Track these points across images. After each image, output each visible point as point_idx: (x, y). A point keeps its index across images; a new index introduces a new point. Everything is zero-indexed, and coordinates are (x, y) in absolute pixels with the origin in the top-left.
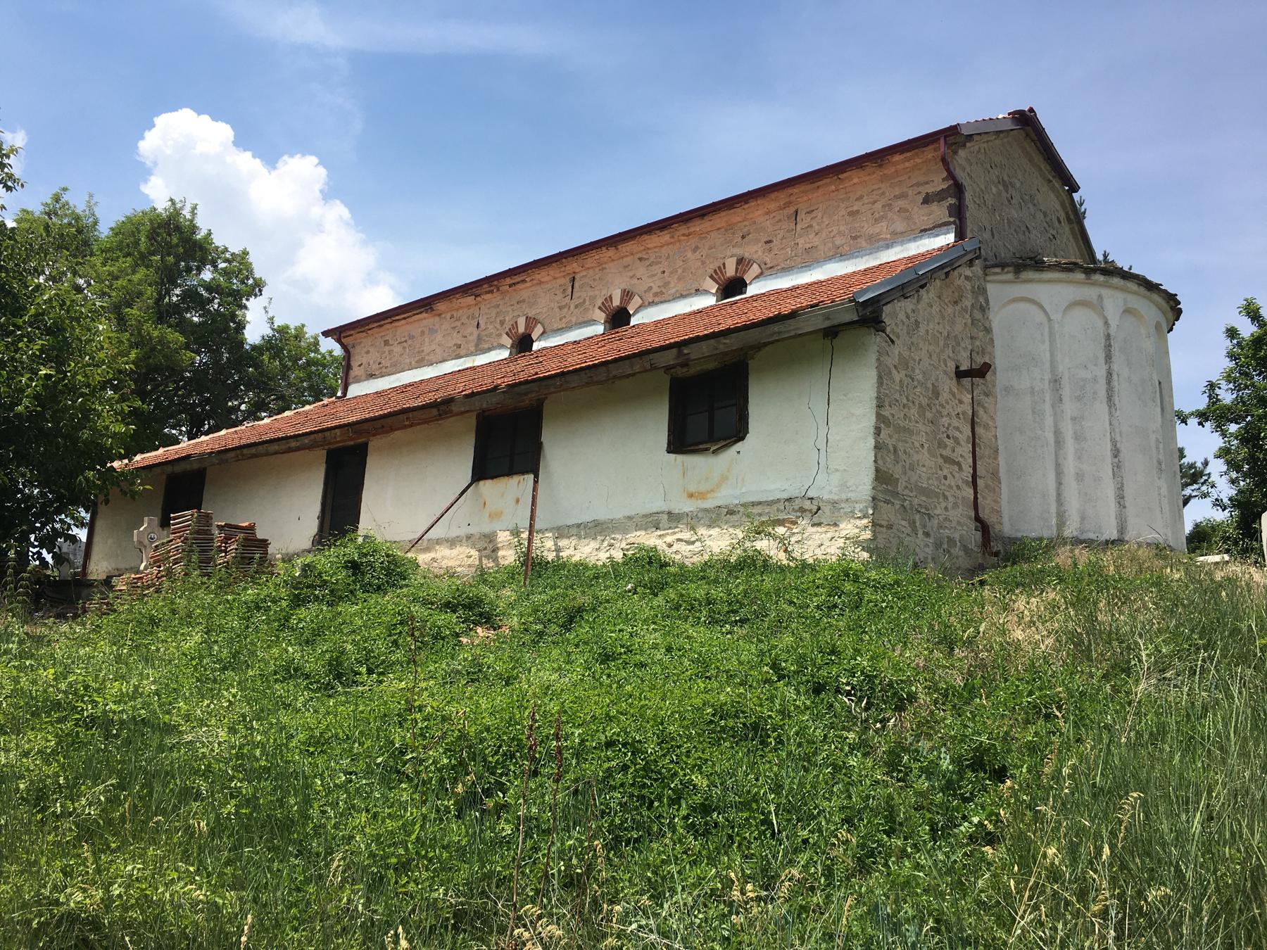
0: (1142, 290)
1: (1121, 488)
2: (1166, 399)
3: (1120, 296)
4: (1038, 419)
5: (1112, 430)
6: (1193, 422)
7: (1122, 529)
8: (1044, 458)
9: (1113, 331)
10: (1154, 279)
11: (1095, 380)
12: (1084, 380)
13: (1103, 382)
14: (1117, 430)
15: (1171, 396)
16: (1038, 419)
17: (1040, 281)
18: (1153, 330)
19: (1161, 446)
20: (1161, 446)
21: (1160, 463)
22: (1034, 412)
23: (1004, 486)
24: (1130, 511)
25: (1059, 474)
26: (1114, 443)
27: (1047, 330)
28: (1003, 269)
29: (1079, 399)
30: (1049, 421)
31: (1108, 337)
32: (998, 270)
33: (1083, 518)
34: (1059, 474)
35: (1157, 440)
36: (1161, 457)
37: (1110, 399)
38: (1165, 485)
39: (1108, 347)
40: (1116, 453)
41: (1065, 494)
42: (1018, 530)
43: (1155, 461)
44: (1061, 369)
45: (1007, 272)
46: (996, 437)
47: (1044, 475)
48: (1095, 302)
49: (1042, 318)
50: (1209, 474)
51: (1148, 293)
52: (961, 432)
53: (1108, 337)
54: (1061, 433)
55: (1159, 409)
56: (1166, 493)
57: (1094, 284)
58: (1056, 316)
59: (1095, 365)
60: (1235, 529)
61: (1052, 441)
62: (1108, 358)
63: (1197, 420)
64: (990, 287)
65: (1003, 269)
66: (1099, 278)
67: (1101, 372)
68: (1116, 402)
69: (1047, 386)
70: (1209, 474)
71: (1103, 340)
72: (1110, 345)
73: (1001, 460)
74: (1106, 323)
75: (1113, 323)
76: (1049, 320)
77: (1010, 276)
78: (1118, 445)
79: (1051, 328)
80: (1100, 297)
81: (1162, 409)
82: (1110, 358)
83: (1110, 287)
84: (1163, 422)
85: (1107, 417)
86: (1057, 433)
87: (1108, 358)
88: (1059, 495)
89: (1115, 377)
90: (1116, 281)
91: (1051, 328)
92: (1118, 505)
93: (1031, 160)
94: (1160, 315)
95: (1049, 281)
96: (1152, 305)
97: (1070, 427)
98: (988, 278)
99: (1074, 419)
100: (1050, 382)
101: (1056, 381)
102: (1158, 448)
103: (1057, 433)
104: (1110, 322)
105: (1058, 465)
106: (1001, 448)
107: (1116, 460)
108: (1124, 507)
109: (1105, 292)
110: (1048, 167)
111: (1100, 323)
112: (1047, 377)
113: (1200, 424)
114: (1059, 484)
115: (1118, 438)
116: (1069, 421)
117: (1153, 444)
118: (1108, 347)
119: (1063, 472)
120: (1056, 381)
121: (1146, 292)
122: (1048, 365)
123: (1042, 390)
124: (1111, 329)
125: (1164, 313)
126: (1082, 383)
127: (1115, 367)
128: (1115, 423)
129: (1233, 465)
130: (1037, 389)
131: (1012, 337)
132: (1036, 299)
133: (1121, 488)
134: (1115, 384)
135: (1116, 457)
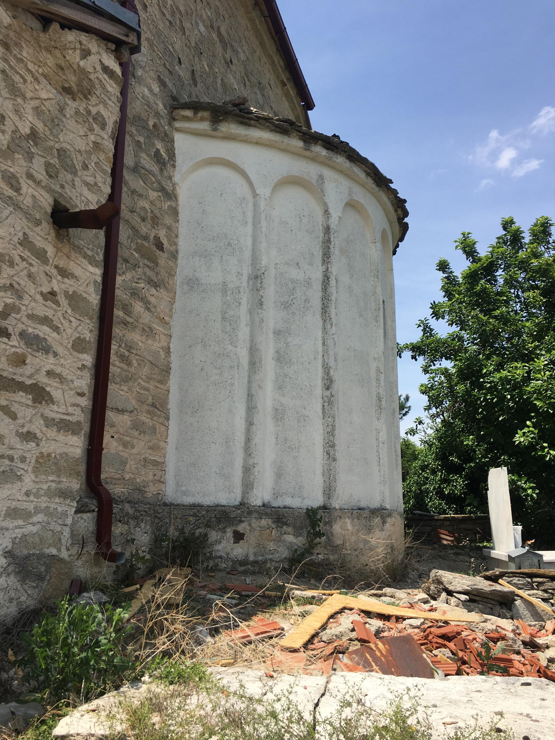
0: (370, 182)
1: (331, 433)
2: (389, 322)
3: (345, 184)
4: (228, 329)
5: (325, 352)
6: (407, 354)
7: (329, 491)
8: (232, 385)
9: (334, 222)
10: (385, 170)
11: (308, 283)
12: (293, 281)
13: (317, 286)
14: (331, 352)
15: (394, 321)
16: (228, 329)
17: (246, 141)
18: (378, 236)
19: (382, 377)
20: (382, 377)
21: (379, 399)
22: (224, 319)
23: (173, 425)
24: (342, 464)
25: (251, 409)
26: (326, 369)
27: (251, 205)
28: (195, 113)
29: (286, 306)
30: (244, 332)
31: (327, 230)
32: (188, 113)
33: (279, 475)
34: (251, 409)
35: (378, 371)
36: (381, 391)
37: (325, 310)
38: (384, 429)
39: (327, 243)
40: (328, 384)
41: (257, 439)
42: (184, 493)
43: (375, 398)
44: (264, 261)
45: (202, 119)
46: (168, 351)
47: (230, 411)
48: (314, 181)
49: (245, 190)
50: (410, 407)
51: (377, 189)
52: (56, 329)
53: (327, 230)
54: (257, 350)
55: (381, 332)
56: (385, 437)
57: (314, 159)
58: (264, 191)
59: (311, 264)
60: (435, 460)
61: (245, 362)
62: (326, 256)
63: (410, 353)
64: (178, 138)
65: (195, 113)
66: (319, 150)
67: (317, 274)
68: (333, 316)
69: (245, 284)
70: (410, 407)
71: (321, 235)
72: (329, 241)
73: (173, 383)
74: (326, 212)
75: (336, 212)
76: (255, 195)
77: (205, 126)
78: (332, 372)
79: (256, 206)
80: (321, 178)
81: (385, 333)
82: (329, 257)
83: (333, 168)
84: (385, 348)
85: (320, 334)
86: (253, 350)
87: (326, 256)
88: (248, 440)
89: (333, 282)
90: (340, 160)
91: (256, 206)
92: (326, 457)
93: (262, 44)
94: (388, 224)
95: (258, 143)
96: (379, 206)
97: (271, 344)
98: (177, 124)
99: (277, 333)
100: (249, 278)
101: (256, 277)
102: (378, 380)
103: (253, 350)
104: (331, 211)
105: (250, 396)
106: (174, 366)
107: (328, 393)
108: (335, 460)
109: (327, 173)
110: (282, 63)
111: (318, 211)
112: (246, 270)
113: (414, 357)
114: (250, 423)
115: (332, 363)
116: (271, 336)
117: (373, 374)
118: (327, 243)
119: (255, 407)
120: (256, 277)
121: (374, 186)
122: (248, 254)
123: (238, 288)
124: (332, 220)
125: (390, 223)
126: (291, 286)
127: (334, 270)
128: (330, 342)
129: (435, 401)
130: (231, 286)
131: (204, 212)
132: (239, 164)
133: (331, 433)
134: (332, 290)
135: (328, 389)
